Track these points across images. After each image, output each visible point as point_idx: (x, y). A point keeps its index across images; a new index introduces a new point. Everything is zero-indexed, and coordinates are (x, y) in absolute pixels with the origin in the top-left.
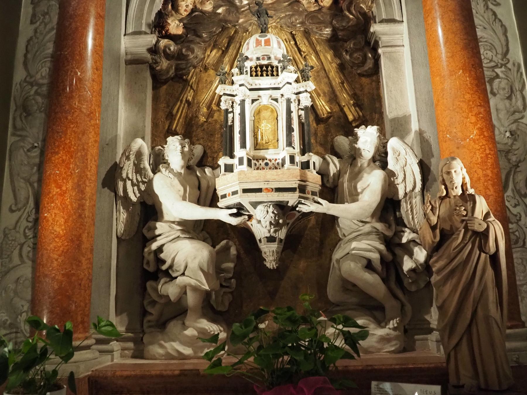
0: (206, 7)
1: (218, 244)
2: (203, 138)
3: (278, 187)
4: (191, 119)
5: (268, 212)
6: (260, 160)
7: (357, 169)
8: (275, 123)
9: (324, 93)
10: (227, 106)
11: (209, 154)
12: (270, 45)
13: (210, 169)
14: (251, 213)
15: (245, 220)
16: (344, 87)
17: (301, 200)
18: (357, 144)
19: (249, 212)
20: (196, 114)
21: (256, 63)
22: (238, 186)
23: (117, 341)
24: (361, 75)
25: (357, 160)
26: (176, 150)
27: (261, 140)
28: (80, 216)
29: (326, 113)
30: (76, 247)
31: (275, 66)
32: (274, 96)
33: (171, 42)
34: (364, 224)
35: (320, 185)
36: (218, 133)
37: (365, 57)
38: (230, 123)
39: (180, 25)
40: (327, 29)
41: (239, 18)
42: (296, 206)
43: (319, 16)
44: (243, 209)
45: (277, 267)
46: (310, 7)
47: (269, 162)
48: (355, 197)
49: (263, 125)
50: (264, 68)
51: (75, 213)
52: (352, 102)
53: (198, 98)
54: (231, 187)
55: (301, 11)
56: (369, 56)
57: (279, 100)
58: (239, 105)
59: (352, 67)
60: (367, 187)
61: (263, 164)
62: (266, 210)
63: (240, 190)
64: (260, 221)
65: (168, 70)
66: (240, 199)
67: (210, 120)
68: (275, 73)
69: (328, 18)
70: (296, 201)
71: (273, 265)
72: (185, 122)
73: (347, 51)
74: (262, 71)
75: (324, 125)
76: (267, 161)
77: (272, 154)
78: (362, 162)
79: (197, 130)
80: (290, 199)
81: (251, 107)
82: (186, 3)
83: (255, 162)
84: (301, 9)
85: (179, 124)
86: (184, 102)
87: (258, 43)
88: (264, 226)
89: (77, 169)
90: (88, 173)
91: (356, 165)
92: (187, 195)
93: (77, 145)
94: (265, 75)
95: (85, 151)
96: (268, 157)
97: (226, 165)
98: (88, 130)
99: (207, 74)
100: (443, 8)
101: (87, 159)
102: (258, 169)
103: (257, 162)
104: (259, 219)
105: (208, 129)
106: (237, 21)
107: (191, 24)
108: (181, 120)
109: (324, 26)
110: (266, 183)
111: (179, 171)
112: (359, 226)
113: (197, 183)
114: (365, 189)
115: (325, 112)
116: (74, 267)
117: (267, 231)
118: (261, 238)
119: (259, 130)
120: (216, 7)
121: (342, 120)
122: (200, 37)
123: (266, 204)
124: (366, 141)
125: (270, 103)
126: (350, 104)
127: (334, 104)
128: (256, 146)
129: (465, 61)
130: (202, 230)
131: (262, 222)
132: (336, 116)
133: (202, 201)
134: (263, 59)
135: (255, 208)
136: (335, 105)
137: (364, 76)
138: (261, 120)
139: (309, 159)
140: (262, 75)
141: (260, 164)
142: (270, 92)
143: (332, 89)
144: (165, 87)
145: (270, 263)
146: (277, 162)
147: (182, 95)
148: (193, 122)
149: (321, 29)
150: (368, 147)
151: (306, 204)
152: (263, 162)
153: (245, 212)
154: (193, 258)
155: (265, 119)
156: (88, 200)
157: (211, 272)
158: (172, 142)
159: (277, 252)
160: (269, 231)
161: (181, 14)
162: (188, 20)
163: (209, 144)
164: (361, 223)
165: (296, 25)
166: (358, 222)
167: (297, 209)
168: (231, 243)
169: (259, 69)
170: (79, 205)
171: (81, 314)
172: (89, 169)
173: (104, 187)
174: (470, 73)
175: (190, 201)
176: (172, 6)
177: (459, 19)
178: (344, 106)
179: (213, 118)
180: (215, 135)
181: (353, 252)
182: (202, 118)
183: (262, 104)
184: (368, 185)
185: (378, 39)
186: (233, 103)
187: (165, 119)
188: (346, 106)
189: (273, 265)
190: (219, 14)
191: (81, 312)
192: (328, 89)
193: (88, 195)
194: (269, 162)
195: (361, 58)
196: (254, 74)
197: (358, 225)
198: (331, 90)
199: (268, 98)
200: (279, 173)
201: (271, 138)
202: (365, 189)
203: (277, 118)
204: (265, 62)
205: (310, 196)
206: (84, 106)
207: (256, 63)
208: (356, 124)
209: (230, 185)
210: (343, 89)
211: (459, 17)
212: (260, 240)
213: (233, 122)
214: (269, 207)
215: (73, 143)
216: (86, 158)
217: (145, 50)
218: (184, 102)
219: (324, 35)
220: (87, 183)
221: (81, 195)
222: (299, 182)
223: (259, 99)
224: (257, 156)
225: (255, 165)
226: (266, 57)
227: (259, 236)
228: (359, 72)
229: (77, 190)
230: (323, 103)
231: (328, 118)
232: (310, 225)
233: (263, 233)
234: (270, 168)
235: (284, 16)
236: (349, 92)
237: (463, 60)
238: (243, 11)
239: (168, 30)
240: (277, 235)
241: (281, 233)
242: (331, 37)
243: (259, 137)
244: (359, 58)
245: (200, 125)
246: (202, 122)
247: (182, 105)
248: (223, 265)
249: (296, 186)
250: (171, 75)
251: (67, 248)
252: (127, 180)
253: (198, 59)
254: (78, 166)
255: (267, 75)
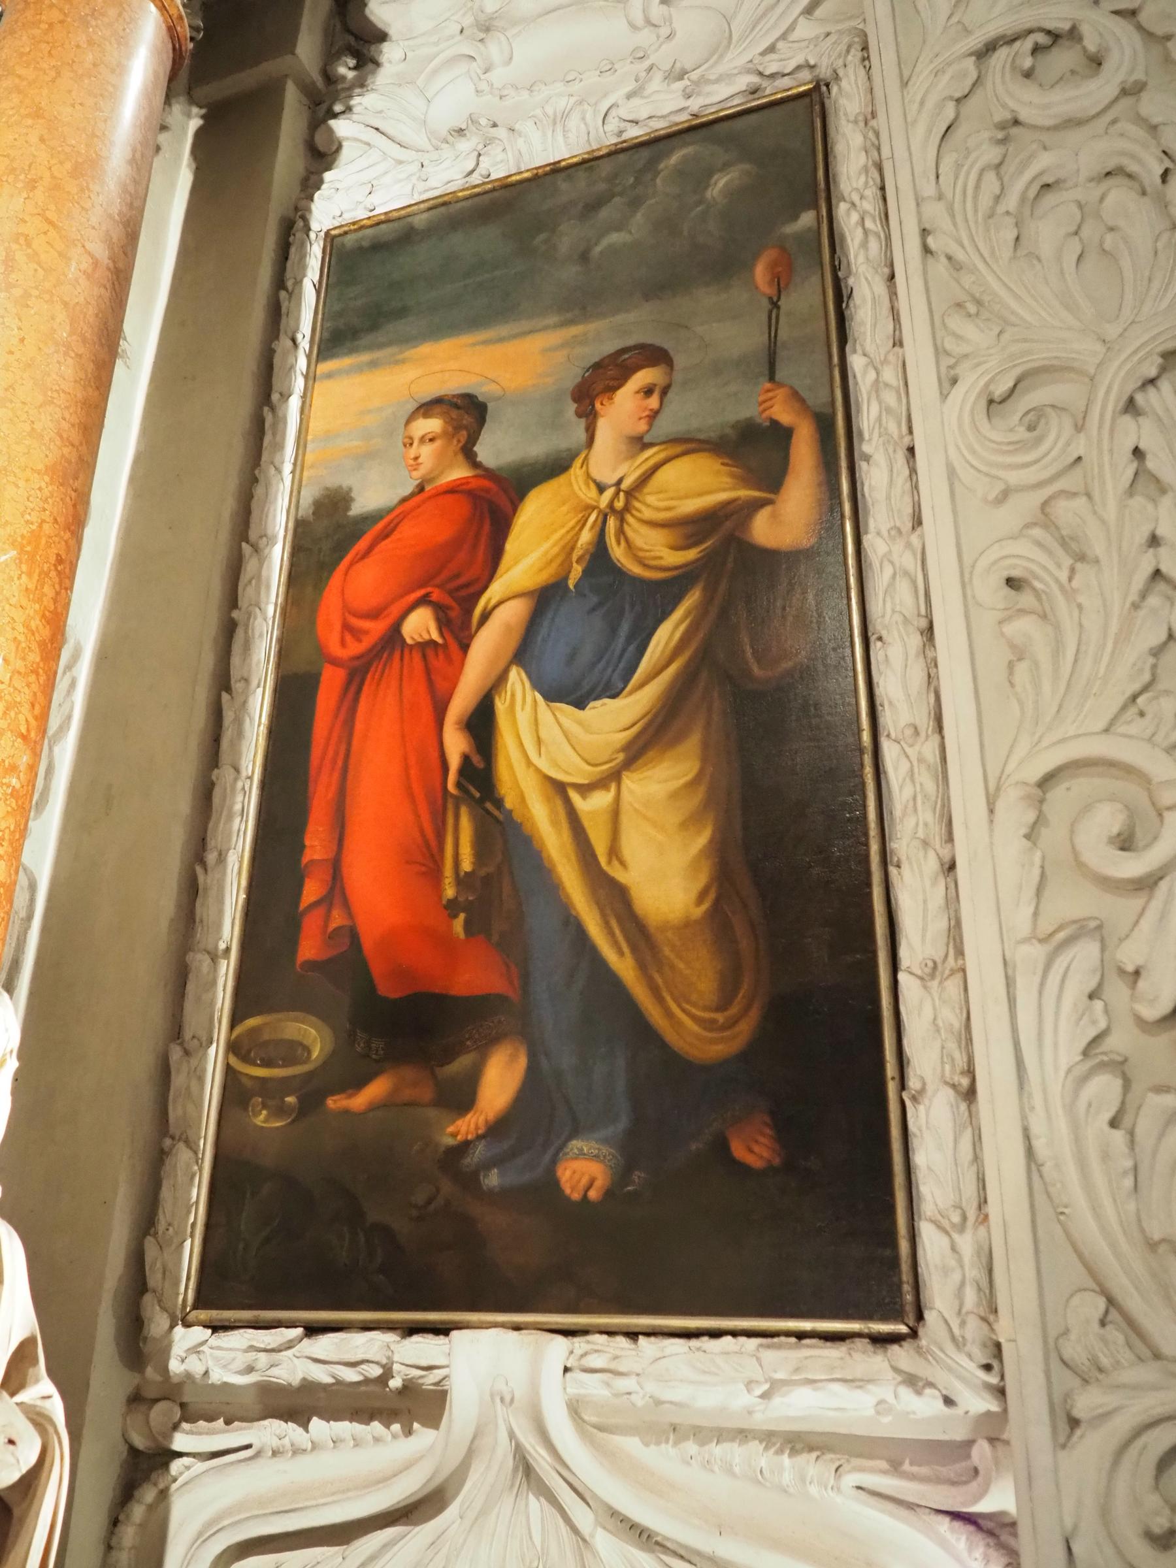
35: (212, 1334)
100: (41, 272)
129: (40, 526)
174: (41, 583)
177: (80, 356)
211: (81, 350)
237: (34, 517)
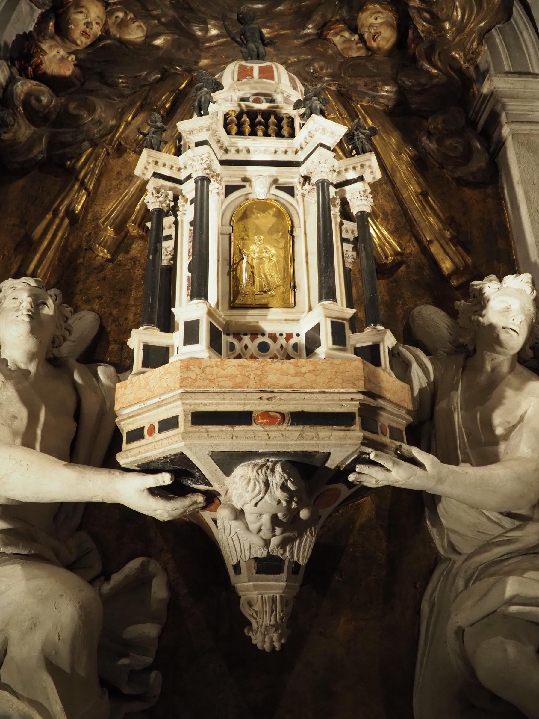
0: (130, 34)
1: (118, 569)
2: (100, 298)
3: (299, 409)
4: (76, 254)
5: (267, 484)
6: (246, 334)
7: (483, 379)
8: (286, 244)
9: (385, 213)
10: (161, 202)
11: (112, 336)
12: (272, 78)
13: (111, 369)
14: (216, 487)
15: (195, 506)
16: (428, 202)
17: (368, 450)
18: (482, 316)
19: (208, 483)
20: (87, 243)
21: (240, 106)
22: (179, 403)
24: (461, 182)
25: (482, 356)
26: (18, 310)
27: (248, 283)
29: (392, 253)
31: (285, 116)
32: (282, 181)
33: (43, 88)
34: (517, 523)
36: (138, 287)
37: (469, 148)
38: (165, 260)
39: (70, 59)
40: (387, 88)
41: (200, 58)
42: (351, 469)
43: (369, 65)
44: (191, 475)
45: (283, 645)
46: (350, 49)
47: (270, 341)
48: (490, 448)
49: (253, 247)
50: (260, 118)
52: (448, 234)
53: (97, 208)
54: (158, 405)
55: (331, 56)
56: (477, 148)
57: (298, 190)
58: (192, 202)
59: (442, 167)
60: (519, 423)
61: (253, 346)
62: (261, 478)
63: (186, 415)
64: (242, 511)
65: (31, 143)
66: (183, 444)
67: (121, 257)
68: (285, 131)
69: (388, 69)
70: (352, 455)
71: (272, 641)
72: (60, 260)
73: (429, 135)
74: (253, 126)
75: (386, 280)
76: (266, 339)
77: (280, 321)
78: (496, 361)
79: (87, 278)
80: (336, 445)
81: (222, 203)
82: (87, 18)
83: (231, 339)
84: (330, 52)
85: (46, 262)
86: (61, 215)
87: (244, 73)
88: (254, 527)
91: (481, 368)
92: (39, 432)
94: (260, 133)
96: (268, 327)
97: (148, 349)
99: (121, 161)
102: (239, 357)
103: (235, 342)
104: (239, 506)
105: (114, 276)
106: (196, 62)
108: (50, 254)
109: (382, 81)
110: (265, 395)
111: (23, 366)
112: (503, 527)
113: (71, 403)
114: (514, 427)
115: (389, 252)
117: (261, 543)
118: (239, 563)
119: (245, 258)
120: (151, 36)
121: (426, 272)
122: (113, 85)
123: (261, 461)
124: (508, 309)
125: (274, 197)
126: (444, 237)
127: (408, 237)
128: (235, 299)
130: (80, 528)
131: (249, 517)
132: (412, 263)
133: (82, 450)
134: (257, 101)
135: (228, 472)
136: (410, 240)
137: (468, 184)
138: (250, 234)
139: (376, 339)
140: (253, 133)
141: (246, 347)
142: (273, 170)
143: (401, 206)
144: (21, 182)
145: (264, 635)
146: (292, 341)
147: (59, 200)
148: (80, 261)
149: (376, 86)
150: (517, 322)
151: (382, 466)
152: (252, 340)
153: (197, 482)
154: (27, 624)
155: (258, 231)
157: (82, 673)
158: (11, 291)
159: (285, 602)
160: (267, 543)
161: (75, 43)
162: (88, 54)
163: (115, 312)
164: (508, 519)
165: (321, 78)
166: (500, 516)
167: (351, 478)
168: (154, 566)
169: (245, 118)
175: (45, 450)
176: (56, 25)
178: (430, 242)
179: (127, 252)
180: (131, 291)
181: (513, 609)
182: (102, 251)
183: (251, 196)
184: (522, 419)
185: (499, 108)
186: (176, 199)
187: (12, 252)
188: (436, 242)
189: (272, 641)
190: (157, 47)
192: (393, 206)
194: (270, 341)
195: (461, 148)
196: (234, 129)
197: (499, 524)
198: (398, 208)
199: (268, 185)
200: (303, 370)
201: (276, 279)
202: (514, 427)
203: (292, 232)
204: (264, 106)
205: (387, 440)
207: (240, 106)
208: (461, 281)
209: (156, 400)
210: (428, 208)
212: (237, 568)
213: (174, 258)
214: (273, 470)
218: (61, 215)
219: (382, 100)
222: (361, 396)
223: (244, 186)
224: (236, 323)
225: (232, 347)
226: (262, 98)
227: (234, 554)
228: (458, 174)
230: (385, 233)
231: (397, 265)
232: (361, 520)
233: (247, 547)
234: (274, 357)
235: (295, 62)
236: (441, 214)
238: (209, 47)
239: (41, 63)
240: (288, 554)
241: (299, 548)
242: (395, 106)
243: (245, 276)
244: (456, 147)
245: (95, 269)
246: (102, 261)
247: (57, 221)
248: (130, 629)
249: (352, 407)
250: (36, 156)
253: (101, 127)
255: (266, 134)
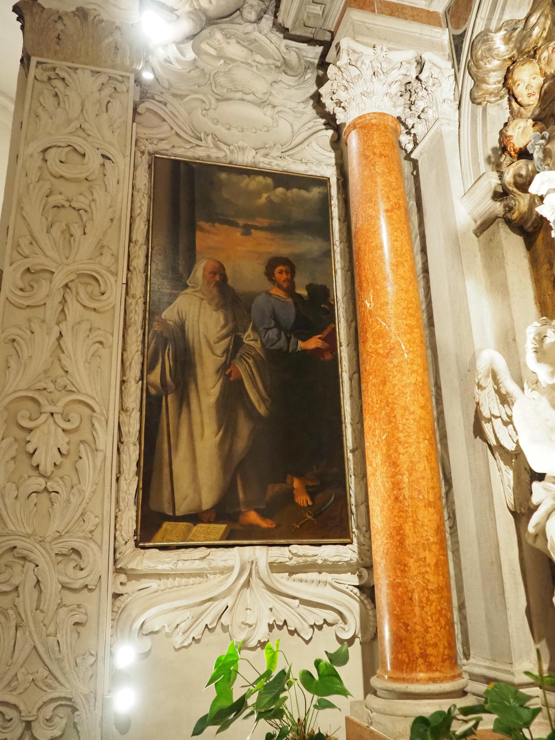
23: (541, 688)
28: (397, 499)
30: (398, 544)
51: (389, 496)
89: (384, 435)
90: (401, 435)
93: (379, 402)
95: (391, 406)
98: (390, 375)
101: (395, 417)
107: (545, 109)
116: (399, 574)
156: (407, 473)
161: (529, 105)
170: (393, 483)
171: (419, 643)
172: (401, 429)
173: (476, 437)
191: (417, 640)
193: (405, 467)
206: (379, 346)
215: (375, 401)
216: (393, 415)
217: (491, 201)
220: (401, 449)
221: (393, 470)
229: (387, 463)
251: (387, 547)
252: (493, 419)
254: (384, 429)
